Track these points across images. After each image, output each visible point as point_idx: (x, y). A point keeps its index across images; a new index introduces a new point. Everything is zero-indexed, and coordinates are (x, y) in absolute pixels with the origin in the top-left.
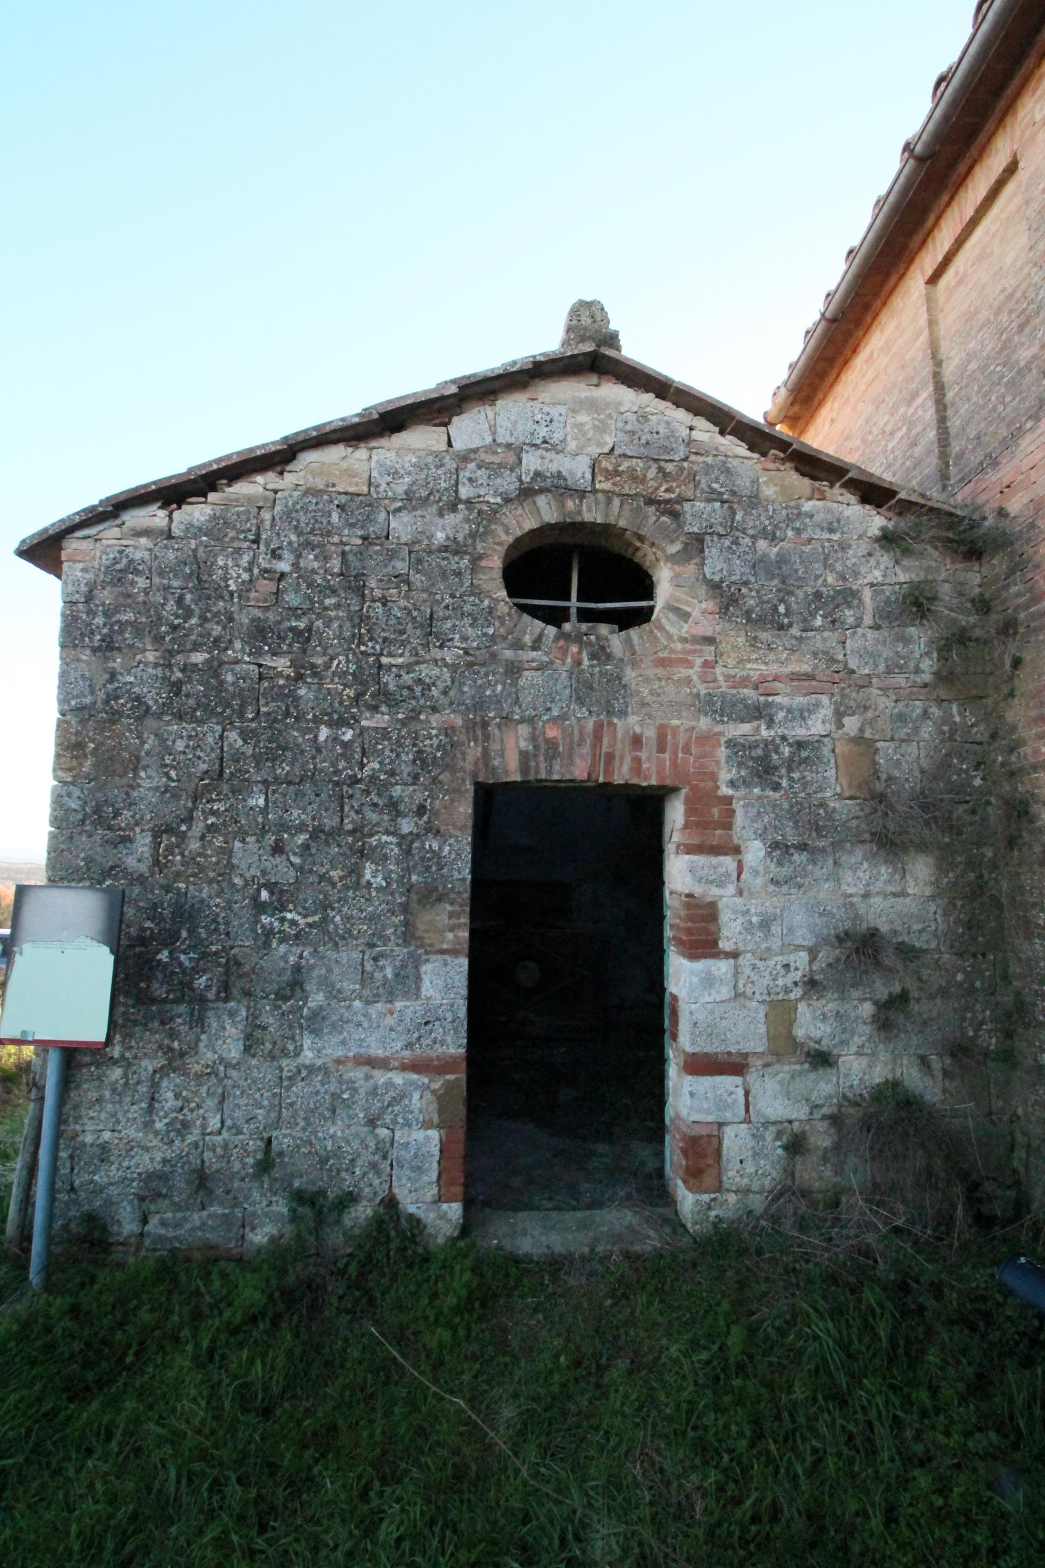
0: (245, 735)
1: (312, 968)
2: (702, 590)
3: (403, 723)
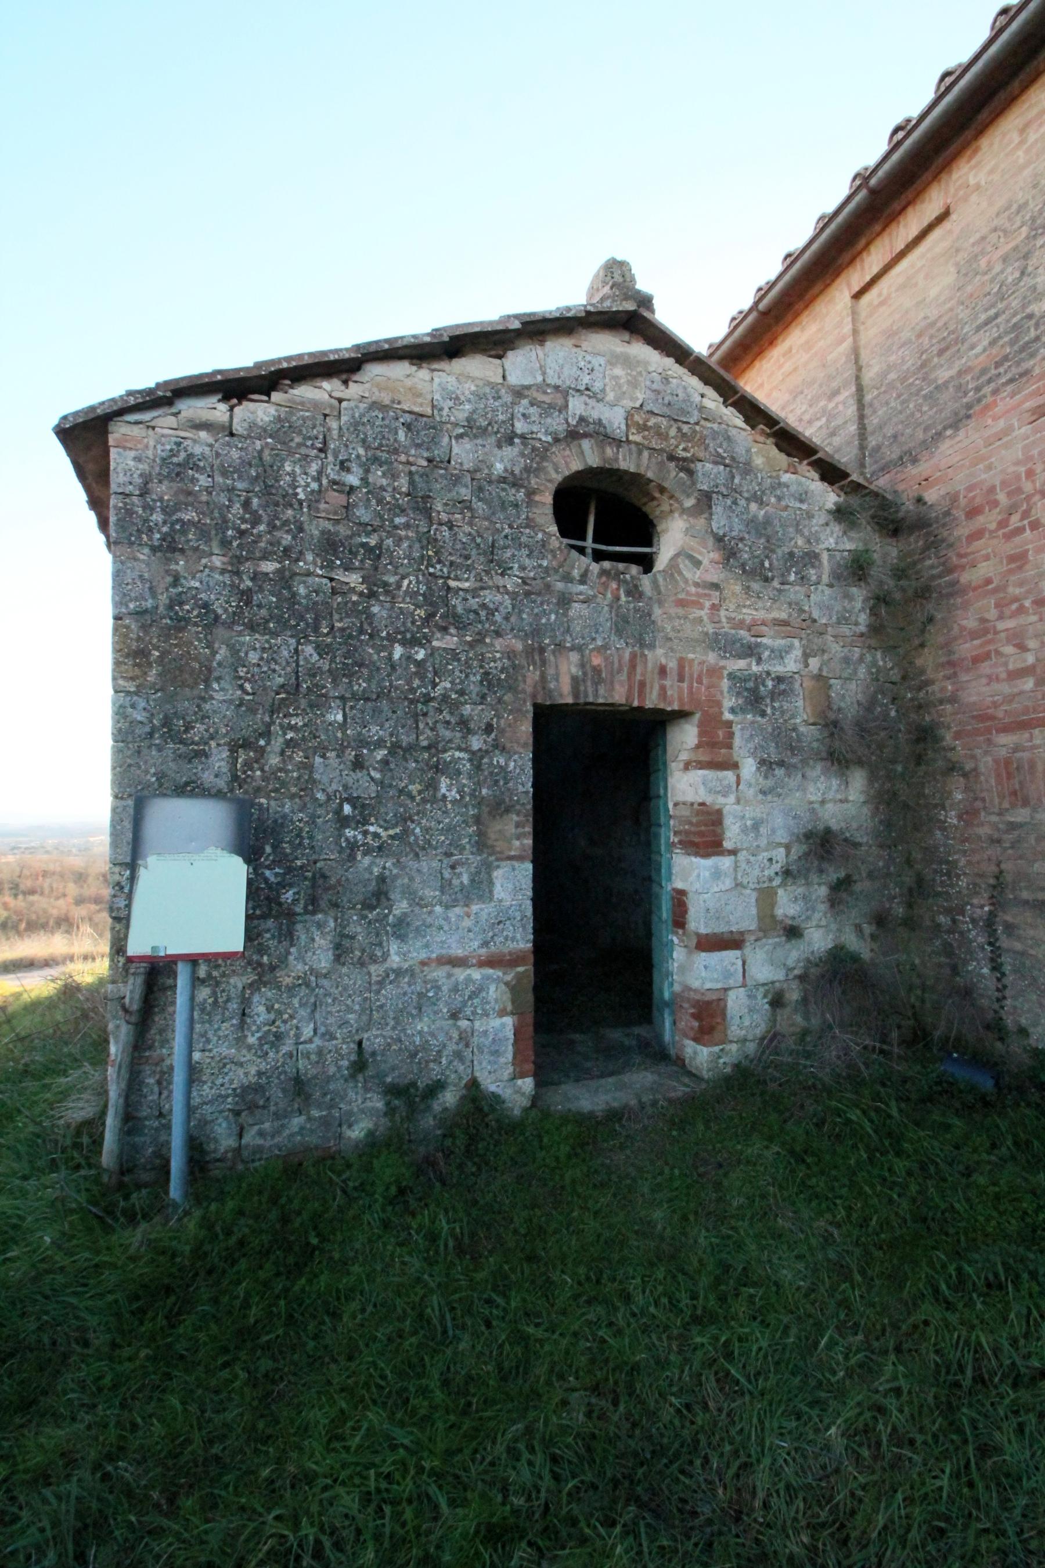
0: (322, 650)
2: (711, 542)
3: (471, 645)
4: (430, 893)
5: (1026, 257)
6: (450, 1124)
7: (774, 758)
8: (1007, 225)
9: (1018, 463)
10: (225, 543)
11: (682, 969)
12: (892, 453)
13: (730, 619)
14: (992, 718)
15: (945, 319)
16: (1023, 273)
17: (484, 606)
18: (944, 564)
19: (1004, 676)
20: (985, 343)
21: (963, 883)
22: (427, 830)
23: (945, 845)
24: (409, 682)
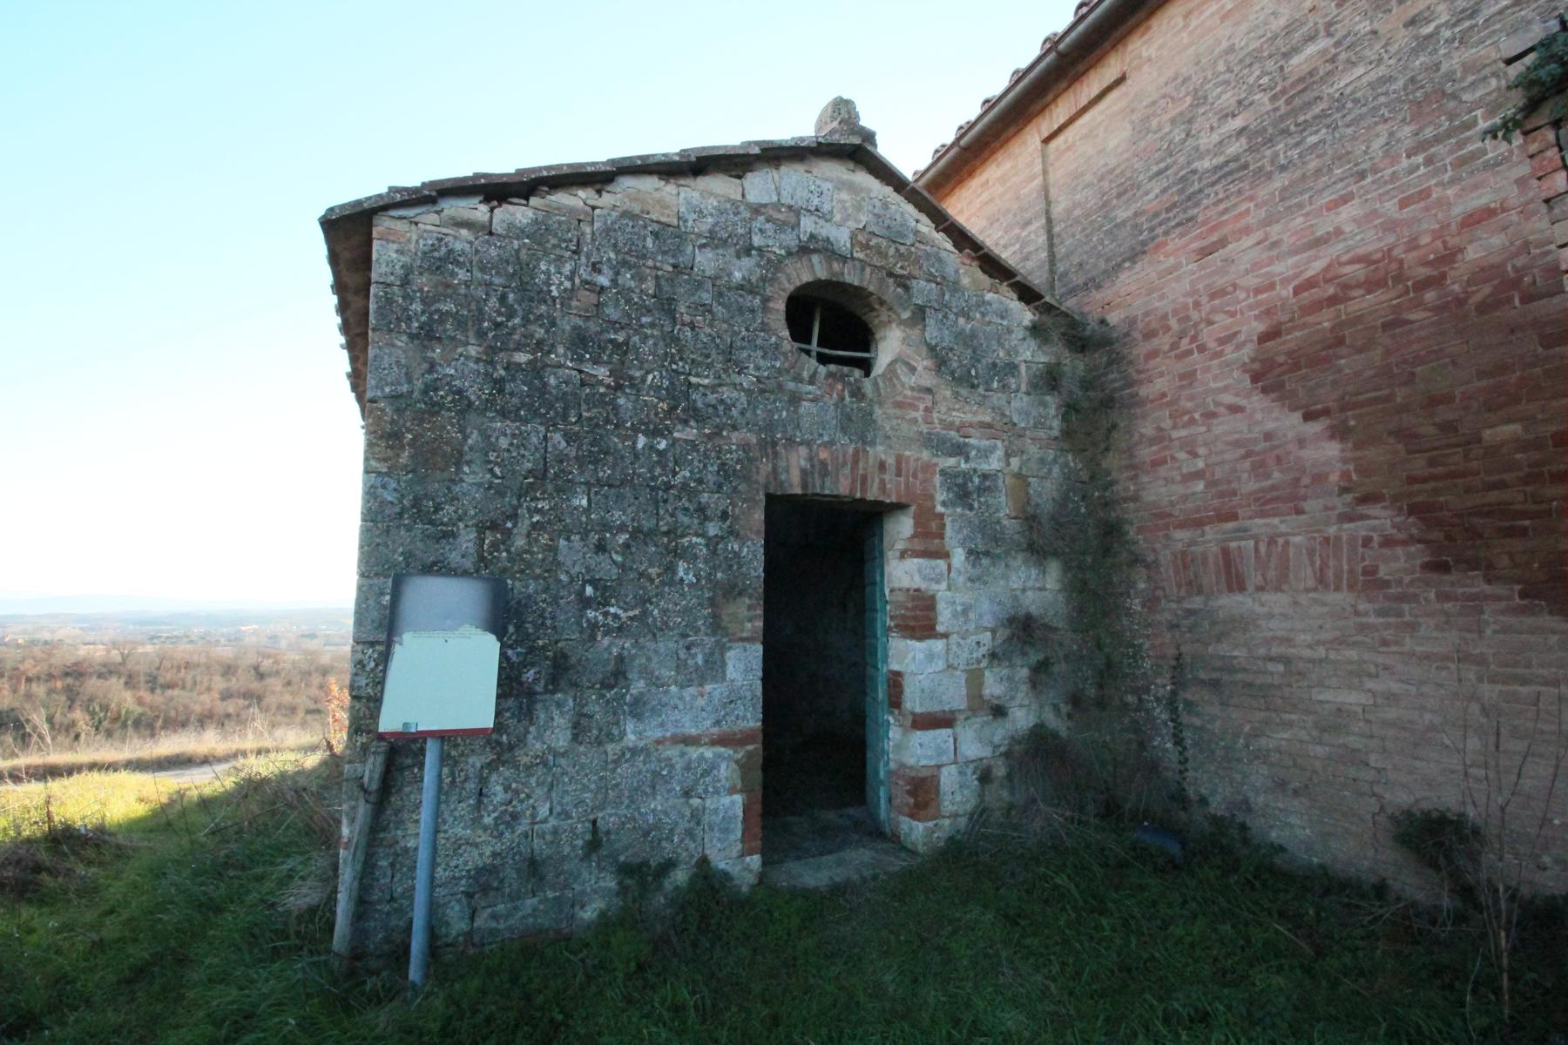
0: (569, 438)
1: (633, 658)
2: (924, 351)
4: (667, 673)
5: (1190, 121)
7: (981, 548)
8: (1174, 94)
9: (1187, 295)
10: (481, 334)
13: (941, 421)
14: (1170, 515)
17: (722, 401)
18: (1124, 378)
21: (1147, 665)
22: (665, 612)
24: (651, 471)
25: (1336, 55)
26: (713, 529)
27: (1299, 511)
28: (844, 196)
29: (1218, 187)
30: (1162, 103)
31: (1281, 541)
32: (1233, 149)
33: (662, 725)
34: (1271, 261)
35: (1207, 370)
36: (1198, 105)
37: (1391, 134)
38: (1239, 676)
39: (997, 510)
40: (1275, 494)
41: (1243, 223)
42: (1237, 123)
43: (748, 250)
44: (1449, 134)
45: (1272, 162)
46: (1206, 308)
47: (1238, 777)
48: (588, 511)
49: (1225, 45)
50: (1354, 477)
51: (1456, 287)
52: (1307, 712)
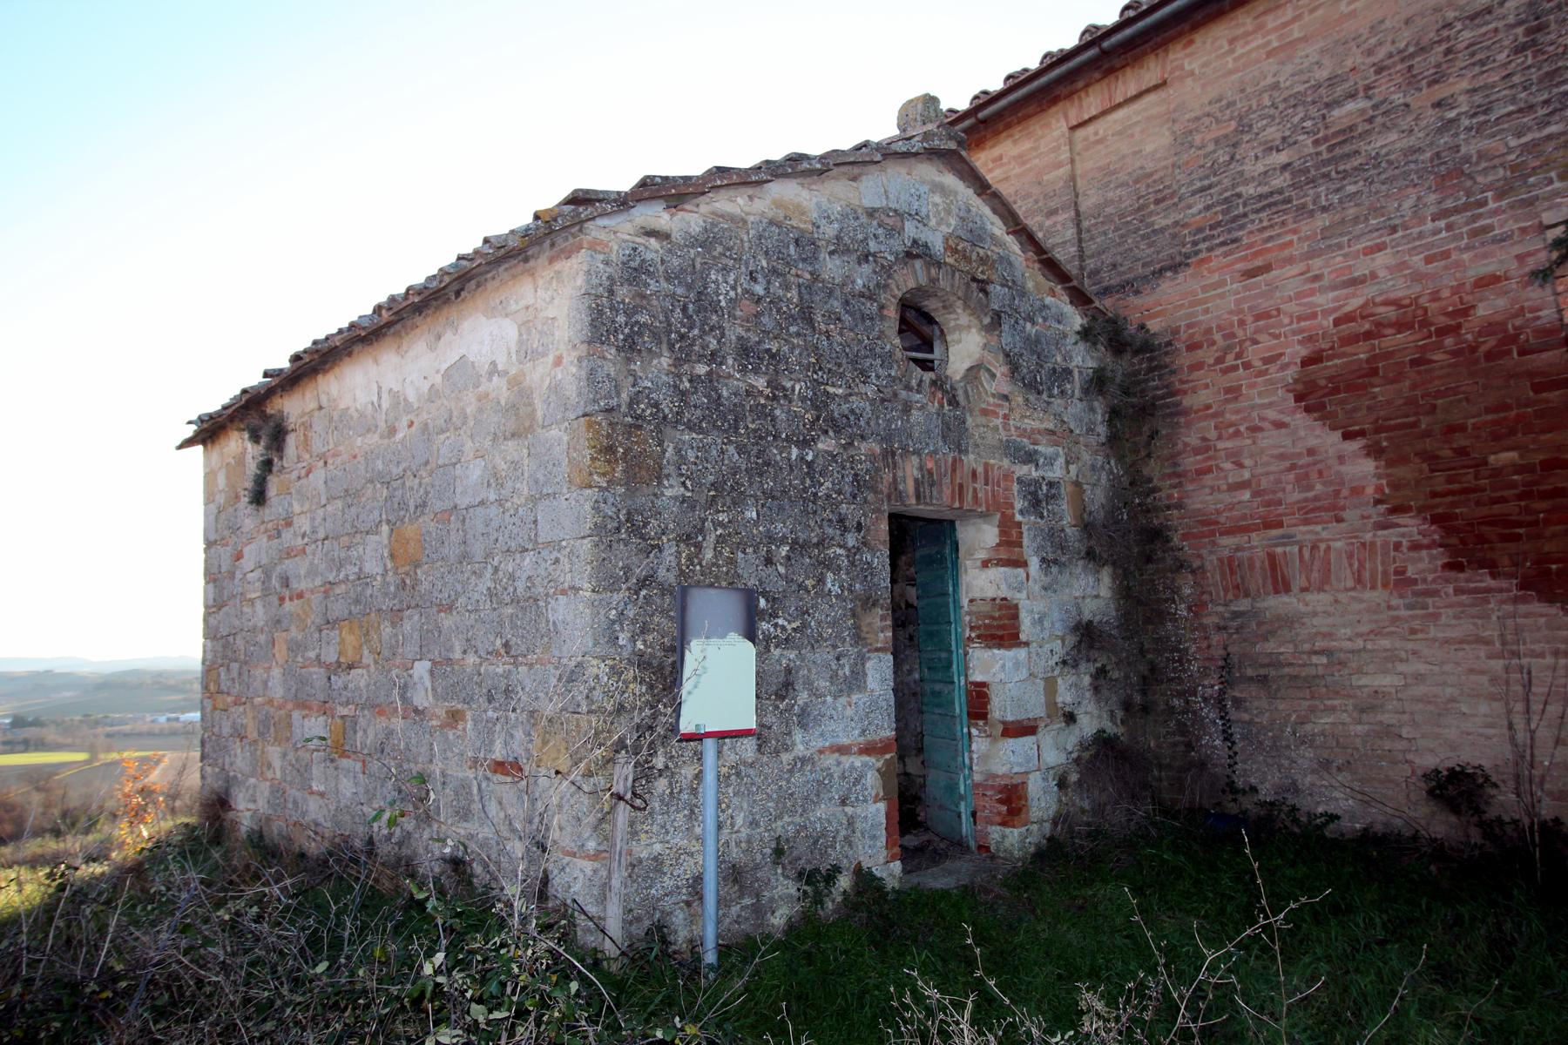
0: (741, 450)
1: (800, 668)
2: (1001, 357)
3: (845, 447)
4: (823, 684)
5: (1235, 145)
6: (851, 903)
7: (1051, 556)
8: (1219, 115)
9: (1231, 312)
10: (671, 347)
11: (985, 758)
12: (1110, 279)
13: (1017, 428)
14: (1217, 523)
15: (1161, 174)
16: (1232, 158)
17: (852, 411)
18: (1167, 387)
19: (1224, 487)
20: (1201, 206)
21: (1194, 667)
22: (819, 623)
23: (1176, 635)
24: (803, 483)
25: (1373, 117)
26: (851, 540)
27: (1339, 520)
28: (937, 199)
29: (1263, 215)
30: (1206, 120)
31: (1323, 546)
32: (1279, 181)
33: (822, 735)
34: (1312, 292)
35: (1252, 386)
36: (1242, 132)
37: (1419, 198)
38: (1286, 670)
39: (1061, 519)
40: (1318, 504)
41: (1287, 252)
42: (1282, 158)
43: (865, 257)
44: (1466, 207)
45: (1314, 203)
46: (1250, 328)
47: (1286, 763)
48: (756, 523)
49: (1270, 80)
50: (1387, 491)
51: (1469, 337)
52: (1349, 696)
